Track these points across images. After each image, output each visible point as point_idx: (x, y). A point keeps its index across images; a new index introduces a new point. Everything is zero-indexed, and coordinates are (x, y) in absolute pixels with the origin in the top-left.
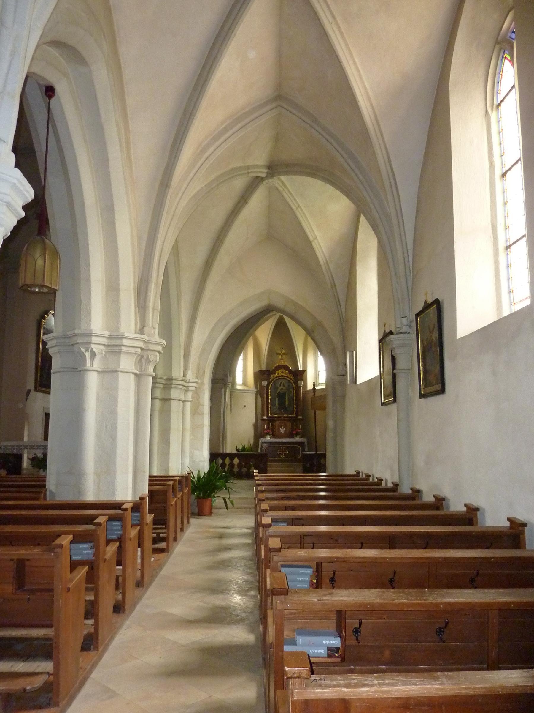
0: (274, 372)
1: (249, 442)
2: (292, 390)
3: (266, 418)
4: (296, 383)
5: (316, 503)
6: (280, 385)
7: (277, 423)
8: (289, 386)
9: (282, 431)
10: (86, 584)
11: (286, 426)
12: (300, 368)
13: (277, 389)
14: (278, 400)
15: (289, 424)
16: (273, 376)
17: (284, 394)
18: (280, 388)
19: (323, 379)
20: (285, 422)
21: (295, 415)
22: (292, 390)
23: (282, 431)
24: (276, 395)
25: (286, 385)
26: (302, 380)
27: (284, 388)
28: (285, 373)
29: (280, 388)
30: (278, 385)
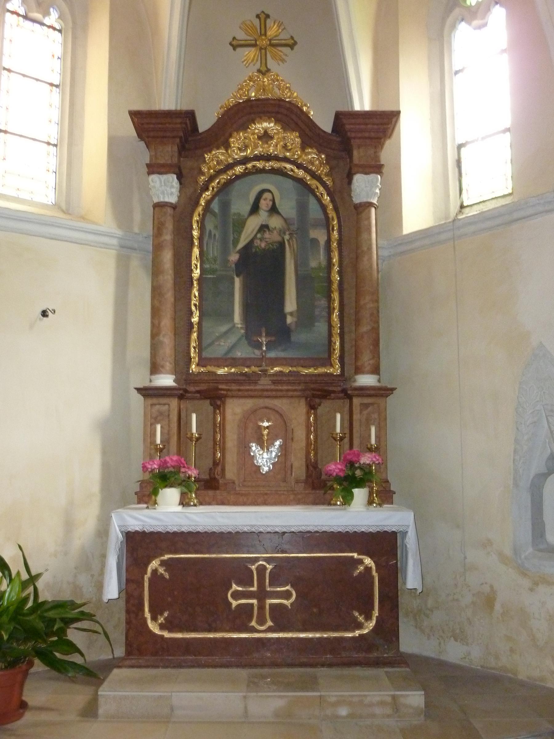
0: (220, 135)
1: (69, 525)
2: (320, 235)
3: (167, 380)
4: (341, 192)
5: (29, 207)
6: (255, 209)
7: (235, 409)
8: (302, 208)
9: (265, 458)
10: (384, 545)
11: (283, 430)
12: (362, 101)
13: (240, 224)
14: (246, 288)
15: (297, 412)
16: (216, 157)
17: (276, 255)
18: (253, 224)
19: (491, 179)
20: (277, 403)
21: (336, 370)
22: (320, 235)
23: (265, 458)
24: (234, 257)
25: (288, 207)
26: (377, 168)
27: (275, 222)
28: (284, 141)
29: (253, 224)
30: (239, 206)
